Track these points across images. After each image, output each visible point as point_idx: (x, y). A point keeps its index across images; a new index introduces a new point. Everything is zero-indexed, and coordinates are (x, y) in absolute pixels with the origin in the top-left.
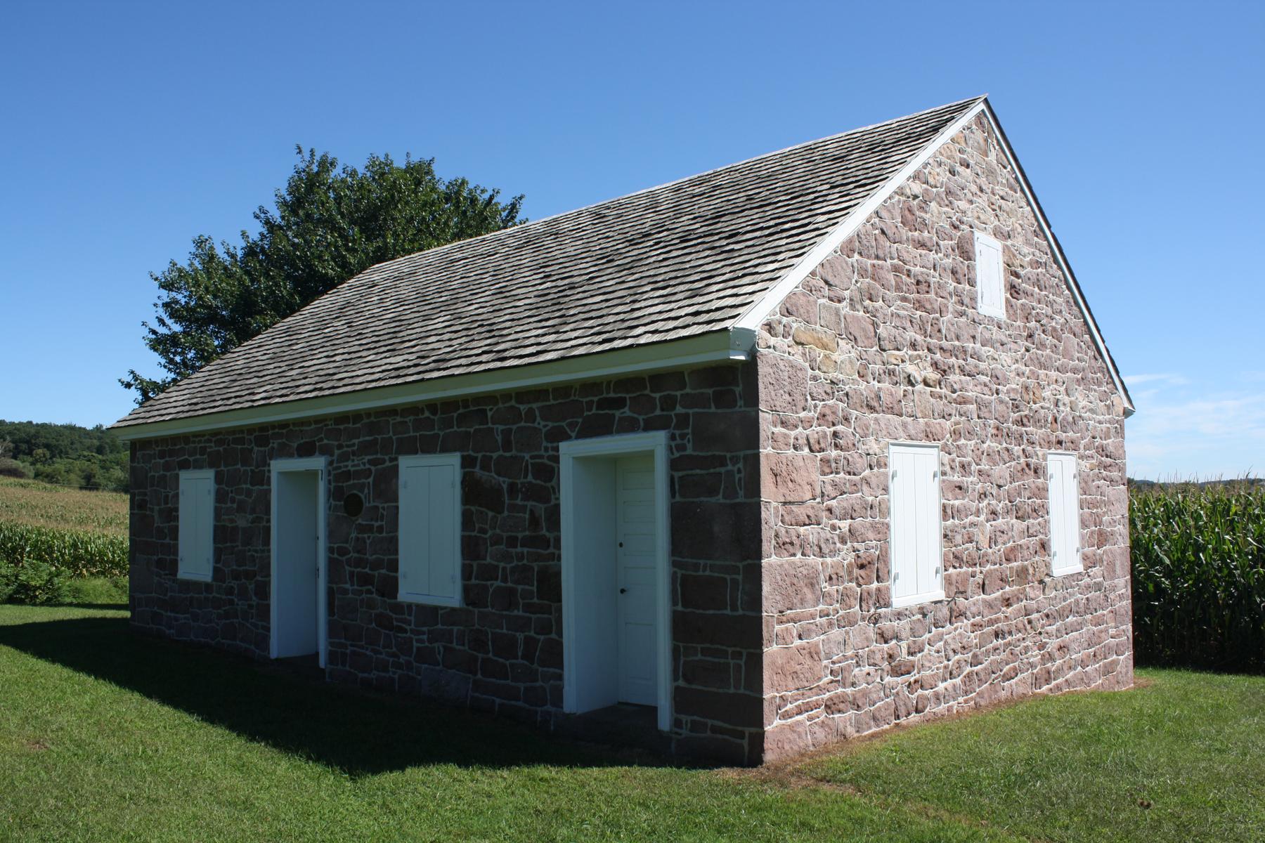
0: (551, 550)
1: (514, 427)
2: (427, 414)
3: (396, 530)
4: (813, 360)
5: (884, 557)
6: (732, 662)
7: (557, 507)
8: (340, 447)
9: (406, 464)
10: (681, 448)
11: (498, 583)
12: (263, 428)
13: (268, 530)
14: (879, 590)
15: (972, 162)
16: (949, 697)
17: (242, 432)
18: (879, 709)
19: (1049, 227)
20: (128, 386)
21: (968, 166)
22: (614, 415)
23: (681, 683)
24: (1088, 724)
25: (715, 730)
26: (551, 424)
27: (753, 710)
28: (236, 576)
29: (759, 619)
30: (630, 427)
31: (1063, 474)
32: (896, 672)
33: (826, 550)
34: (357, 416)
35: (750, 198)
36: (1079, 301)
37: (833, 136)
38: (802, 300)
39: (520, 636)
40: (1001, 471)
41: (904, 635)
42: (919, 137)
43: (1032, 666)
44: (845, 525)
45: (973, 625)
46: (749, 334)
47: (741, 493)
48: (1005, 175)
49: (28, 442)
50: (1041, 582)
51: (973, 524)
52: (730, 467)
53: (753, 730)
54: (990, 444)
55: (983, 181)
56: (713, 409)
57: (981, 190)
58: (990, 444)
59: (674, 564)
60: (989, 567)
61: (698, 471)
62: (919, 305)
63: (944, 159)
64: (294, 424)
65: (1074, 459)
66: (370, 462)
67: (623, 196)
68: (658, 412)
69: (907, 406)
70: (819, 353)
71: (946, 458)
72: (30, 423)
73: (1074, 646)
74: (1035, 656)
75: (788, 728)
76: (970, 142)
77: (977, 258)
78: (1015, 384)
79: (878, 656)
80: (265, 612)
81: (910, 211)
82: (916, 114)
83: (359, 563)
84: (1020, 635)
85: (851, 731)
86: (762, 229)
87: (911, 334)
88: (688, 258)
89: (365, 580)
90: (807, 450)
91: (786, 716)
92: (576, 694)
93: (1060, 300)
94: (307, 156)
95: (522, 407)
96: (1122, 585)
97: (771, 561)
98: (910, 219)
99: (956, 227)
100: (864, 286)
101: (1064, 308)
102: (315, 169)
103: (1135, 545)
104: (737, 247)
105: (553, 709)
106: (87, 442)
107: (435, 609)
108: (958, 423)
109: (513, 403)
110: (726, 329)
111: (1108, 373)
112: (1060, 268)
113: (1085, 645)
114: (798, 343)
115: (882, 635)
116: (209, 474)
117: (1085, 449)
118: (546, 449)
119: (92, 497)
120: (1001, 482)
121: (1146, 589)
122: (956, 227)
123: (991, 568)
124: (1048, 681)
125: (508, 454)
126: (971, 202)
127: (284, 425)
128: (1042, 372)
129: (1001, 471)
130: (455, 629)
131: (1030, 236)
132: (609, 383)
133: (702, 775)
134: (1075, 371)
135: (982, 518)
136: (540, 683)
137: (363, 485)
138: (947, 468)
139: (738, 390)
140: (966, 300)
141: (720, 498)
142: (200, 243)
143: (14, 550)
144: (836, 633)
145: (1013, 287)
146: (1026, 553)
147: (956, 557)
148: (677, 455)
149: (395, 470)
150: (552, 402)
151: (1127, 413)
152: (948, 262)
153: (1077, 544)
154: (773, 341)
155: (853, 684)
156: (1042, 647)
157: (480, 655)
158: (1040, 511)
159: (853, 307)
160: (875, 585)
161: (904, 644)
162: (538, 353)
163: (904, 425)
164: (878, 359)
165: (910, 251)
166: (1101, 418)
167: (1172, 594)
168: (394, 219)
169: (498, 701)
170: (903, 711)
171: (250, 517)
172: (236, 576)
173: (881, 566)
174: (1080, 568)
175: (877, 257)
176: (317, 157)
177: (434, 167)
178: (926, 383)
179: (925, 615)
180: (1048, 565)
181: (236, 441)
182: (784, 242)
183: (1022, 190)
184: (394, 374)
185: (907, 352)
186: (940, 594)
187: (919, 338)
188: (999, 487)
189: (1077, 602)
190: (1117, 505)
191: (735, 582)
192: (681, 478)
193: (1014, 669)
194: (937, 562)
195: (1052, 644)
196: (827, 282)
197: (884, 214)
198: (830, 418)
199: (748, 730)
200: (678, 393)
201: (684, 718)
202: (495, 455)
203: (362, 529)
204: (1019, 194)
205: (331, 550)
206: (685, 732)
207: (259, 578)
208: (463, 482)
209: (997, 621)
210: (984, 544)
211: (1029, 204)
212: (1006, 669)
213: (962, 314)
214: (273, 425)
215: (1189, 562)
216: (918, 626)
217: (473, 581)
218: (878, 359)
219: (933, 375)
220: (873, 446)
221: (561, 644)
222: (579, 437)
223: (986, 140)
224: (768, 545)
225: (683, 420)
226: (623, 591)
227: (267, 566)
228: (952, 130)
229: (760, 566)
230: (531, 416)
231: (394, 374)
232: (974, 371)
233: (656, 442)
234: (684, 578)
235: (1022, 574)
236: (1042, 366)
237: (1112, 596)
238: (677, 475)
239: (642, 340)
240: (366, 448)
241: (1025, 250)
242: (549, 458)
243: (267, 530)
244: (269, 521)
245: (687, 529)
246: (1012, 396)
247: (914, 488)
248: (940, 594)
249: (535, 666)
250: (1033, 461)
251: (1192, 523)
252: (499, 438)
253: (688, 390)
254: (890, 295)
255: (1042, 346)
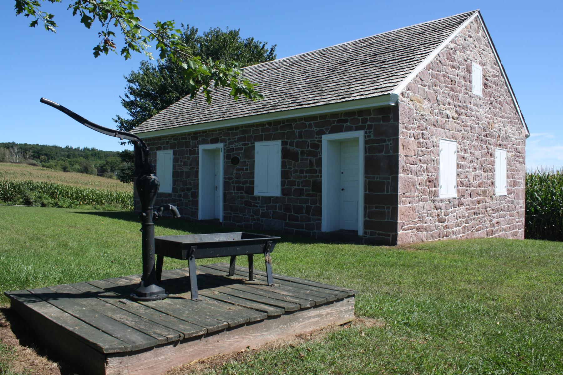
0: (318, 174)
1: (303, 130)
2: (267, 126)
3: (254, 169)
4: (416, 107)
5: (437, 179)
6: (386, 210)
7: (320, 159)
8: (229, 139)
9: (257, 144)
10: (369, 136)
11: (296, 187)
12: (195, 133)
13: (197, 172)
14: (435, 190)
15: (472, 36)
16: (457, 234)
17: (186, 135)
18: (434, 233)
19: (500, 61)
20: (116, 121)
21: (471, 37)
22: (343, 125)
23: (367, 219)
24: (508, 245)
25: (379, 234)
26: (318, 129)
27: (394, 227)
28: (183, 190)
29: (397, 196)
30: (350, 129)
31: (501, 157)
32: (440, 221)
33: (418, 174)
34: (237, 128)
35: (387, 48)
36: (510, 91)
37: (418, 24)
38: (413, 85)
39: (304, 206)
40: (478, 153)
41: (443, 208)
42: (453, 26)
43: (487, 227)
44: (425, 166)
45: (467, 209)
46: (396, 96)
47: (391, 152)
48: (484, 41)
49: (38, 153)
50: (491, 197)
51: (468, 172)
52: (387, 143)
53: (393, 233)
54: (474, 143)
55: (476, 43)
56: (382, 123)
57: (475, 47)
58: (474, 143)
59: (366, 177)
60: (473, 188)
61: (375, 144)
62: (452, 89)
63: (462, 35)
64: (209, 131)
65: (505, 152)
66: (242, 145)
67: (332, 46)
68: (360, 124)
69: (446, 126)
70: (418, 105)
71: (459, 146)
72: (38, 144)
73: (502, 223)
74: (488, 224)
75: (404, 235)
76: (472, 28)
77: (473, 72)
78: (485, 121)
79: (434, 214)
80: (196, 203)
81: (450, 54)
82: (451, 16)
83: (237, 182)
84: (483, 215)
85: (424, 239)
86: (395, 60)
87: (449, 100)
88: (367, 70)
89: (239, 188)
90: (413, 138)
91: (404, 230)
92: (326, 226)
93: (503, 90)
94: (186, 28)
95: (307, 123)
96: (522, 203)
97: (401, 175)
98: (450, 57)
99: (466, 61)
100: (433, 81)
101: (504, 93)
102: (189, 33)
103: (527, 192)
104: (386, 66)
105: (317, 231)
106: (63, 153)
107: (269, 198)
108: (463, 134)
109: (303, 121)
110: (389, 94)
111: (521, 120)
112: (503, 77)
113: (506, 223)
114: (412, 100)
115: (435, 207)
116: (171, 152)
117: (510, 149)
118: (316, 138)
119: (68, 175)
120: (478, 157)
121: (530, 210)
122: (466, 61)
123: (474, 189)
124: (492, 234)
125: (301, 140)
126: (472, 51)
127: (204, 132)
128: (495, 117)
129: (478, 153)
130: (278, 205)
131: (493, 65)
132: (342, 114)
133: (378, 248)
134: (507, 118)
135: (471, 170)
136: (312, 222)
137: (240, 153)
138: (459, 150)
139: (391, 116)
140: (468, 89)
141: (383, 154)
142: (143, 64)
143: (53, 193)
144: (421, 204)
145: (485, 84)
146: (486, 185)
147: (461, 183)
148: (367, 139)
149: (253, 147)
150: (319, 121)
151: (527, 136)
152: (462, 74)
153: (505, 184)
154: (403, 99)
155: (426, 223)
156: (491, 221)
157: (288, 214)
158: (492, 170)
159: (429, 89)
160: (434, 189)
161: (443, 211)
162: (315, 103)
163: (445, 133)
164: (437, 108)
165: (449, 69)
166: (516, 137)
167: (542, 212)
168: (224, 54)
169: (295, 229)
170: (441, 236)
171: (189, 167)
172: (183, 190)
173: (436, 182)
174: (506, 193)
175: (438, 71)
176: (190, 27)
177: (239, 32)
178: (453, 118)
179: (450, 202)
180: (494, 191)
181: (183, 139)
182: (405, 64)
183: (491, 47)
184: (255, 111)
185: (447, 106)
186: (456, 196)
187: (451, 101)
188: (478, 159)
189: (504, 206)
190: (521, 172)
191: (388, 183)
192: (369, 147)
193: (480, 227)
194: (455, 184)
195: (494, 221)
196: (421, 79)
197: (441, 55)
198: (421, 128)
199: (391, 234)
200: (369, 117)
201: (368, 231)
202: (295, 141)
203: (239, 170)
204: (490, 48)
205: (225, 178)
206: (368, 236)
207: (193, 190)
208: (282, 151)
209: (475, 208)
210: (471, 179)
211: (493, 52)
212: (477, 227)
213: (467, 93)
214: (199, 132)
215: (549, 199)
216: (448, 206)
217: (286, 187)
218: (437, 108)
219: (456, 116)
220: (435, 140)
221: (321, 208)
222: (329, 133)
223: (478, 27)
224: (400, 170)
225: (370, 127)
226: (343, 189)
227: (196, 186)
228: (466, 23)
229: (398, 177)
230: (310, 126)
231: (255, 111)
232: (470, 115)
233: (360, 134)
234: (369, 181)
235: (484, 192)
236: (495, 115)
237: (517, 206)
238: (367, 146)
239: (357, 98)
240: (240, 140)
241: (491, 70)
242: (318, 141)
243: (197, 172)
244: (198, 168)
245: (371, 165)
246: (484, 125)
247: (448, 154)
248: (456, 196)
249: (310, 216)
250: (490, 151)
251: (551, 184)
252: (297, 134)
253: (372, 116)
254: (442, 85)
255: (495, 107)
